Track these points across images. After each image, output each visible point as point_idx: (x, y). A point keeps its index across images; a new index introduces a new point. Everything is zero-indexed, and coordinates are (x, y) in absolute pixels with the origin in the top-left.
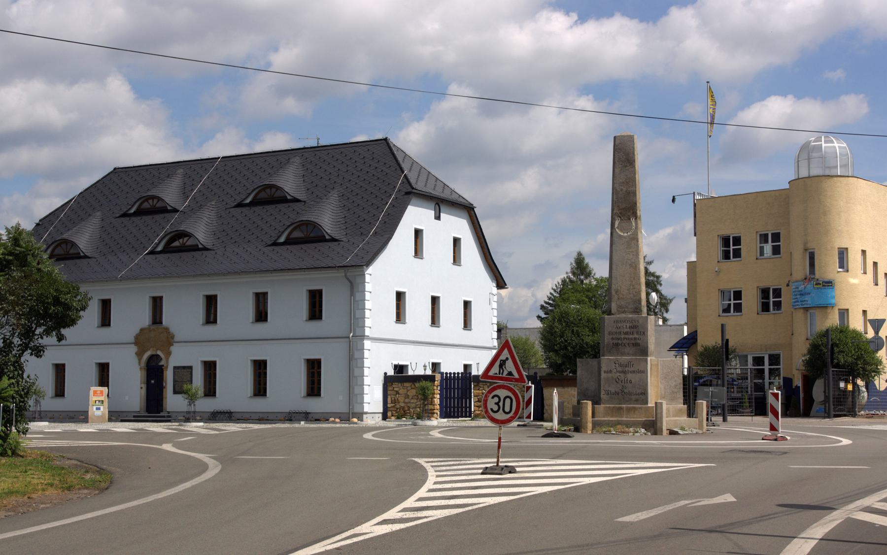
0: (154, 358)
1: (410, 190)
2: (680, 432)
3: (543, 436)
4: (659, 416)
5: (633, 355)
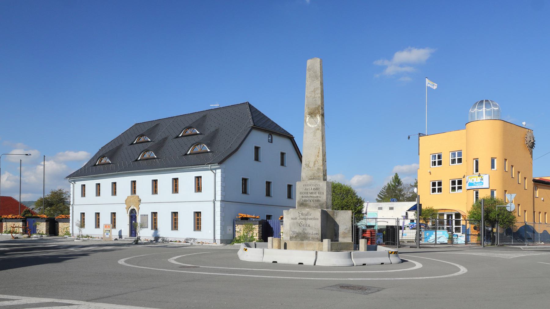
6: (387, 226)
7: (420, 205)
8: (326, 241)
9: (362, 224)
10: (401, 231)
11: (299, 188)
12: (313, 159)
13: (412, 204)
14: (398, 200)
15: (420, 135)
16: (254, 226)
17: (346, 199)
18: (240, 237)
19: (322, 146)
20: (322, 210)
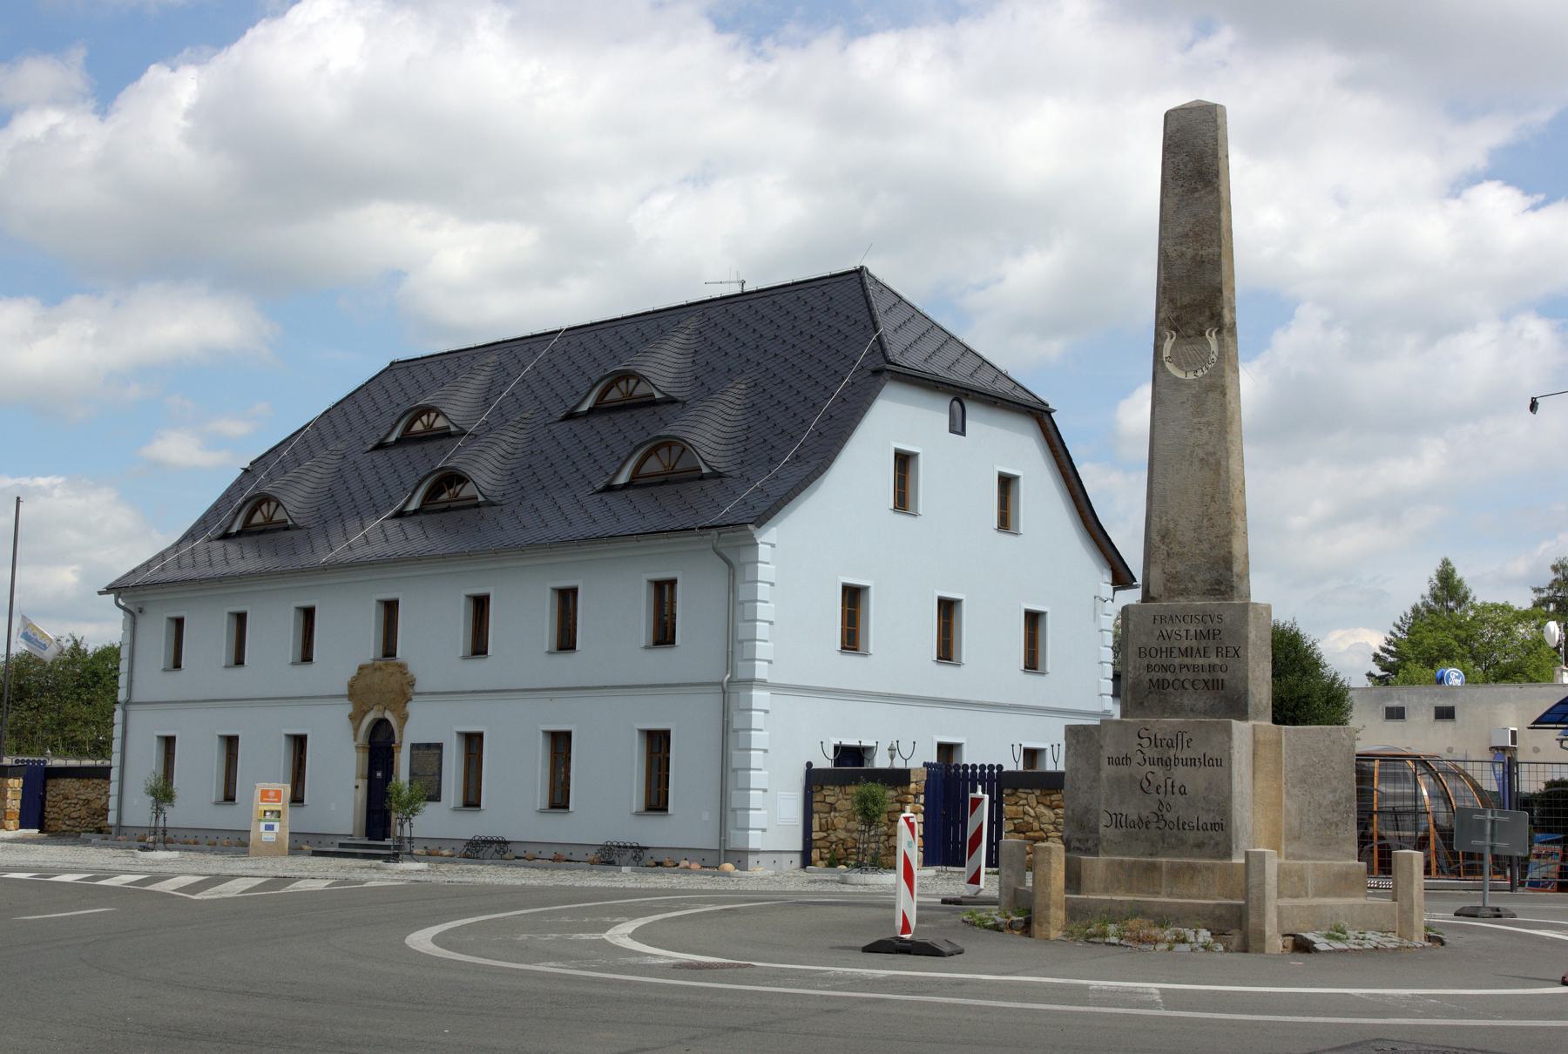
0: (380, 725)
1: (882, 364)
2: (1321, 944)
3: (869, 949)
4: (1254, 893)
5: (1205, 714)
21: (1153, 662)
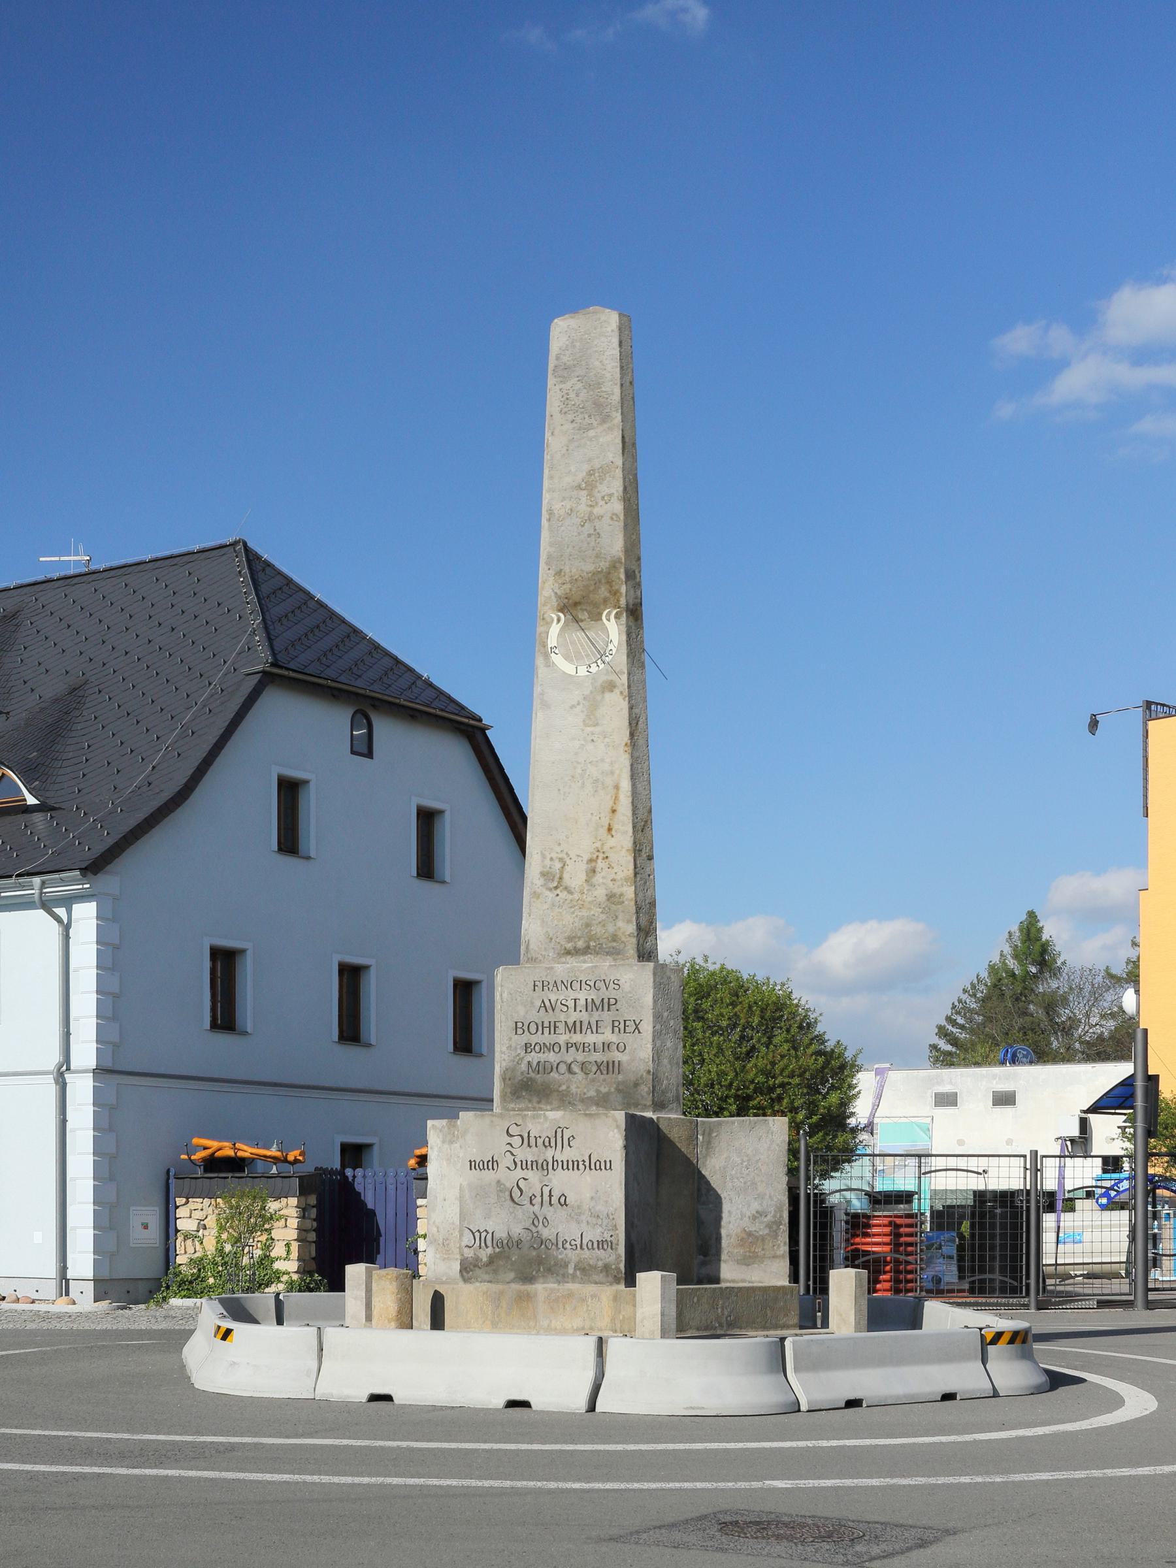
6: (980, 1196)
7: (1153, 1080)
8: (651, 1282)
9: (845, 1188)
10: (1049, 1220)
11: (509, 997)
12: (582, 845)
13: (1115, 1073)
14: (1042, 1056)
15: (1152, 709)
16: (273, 1206)
17: (757, 1053)
18: (199, 1263)
19: (633, 777)
20: (631, 1120)
21: (534, 1039)
